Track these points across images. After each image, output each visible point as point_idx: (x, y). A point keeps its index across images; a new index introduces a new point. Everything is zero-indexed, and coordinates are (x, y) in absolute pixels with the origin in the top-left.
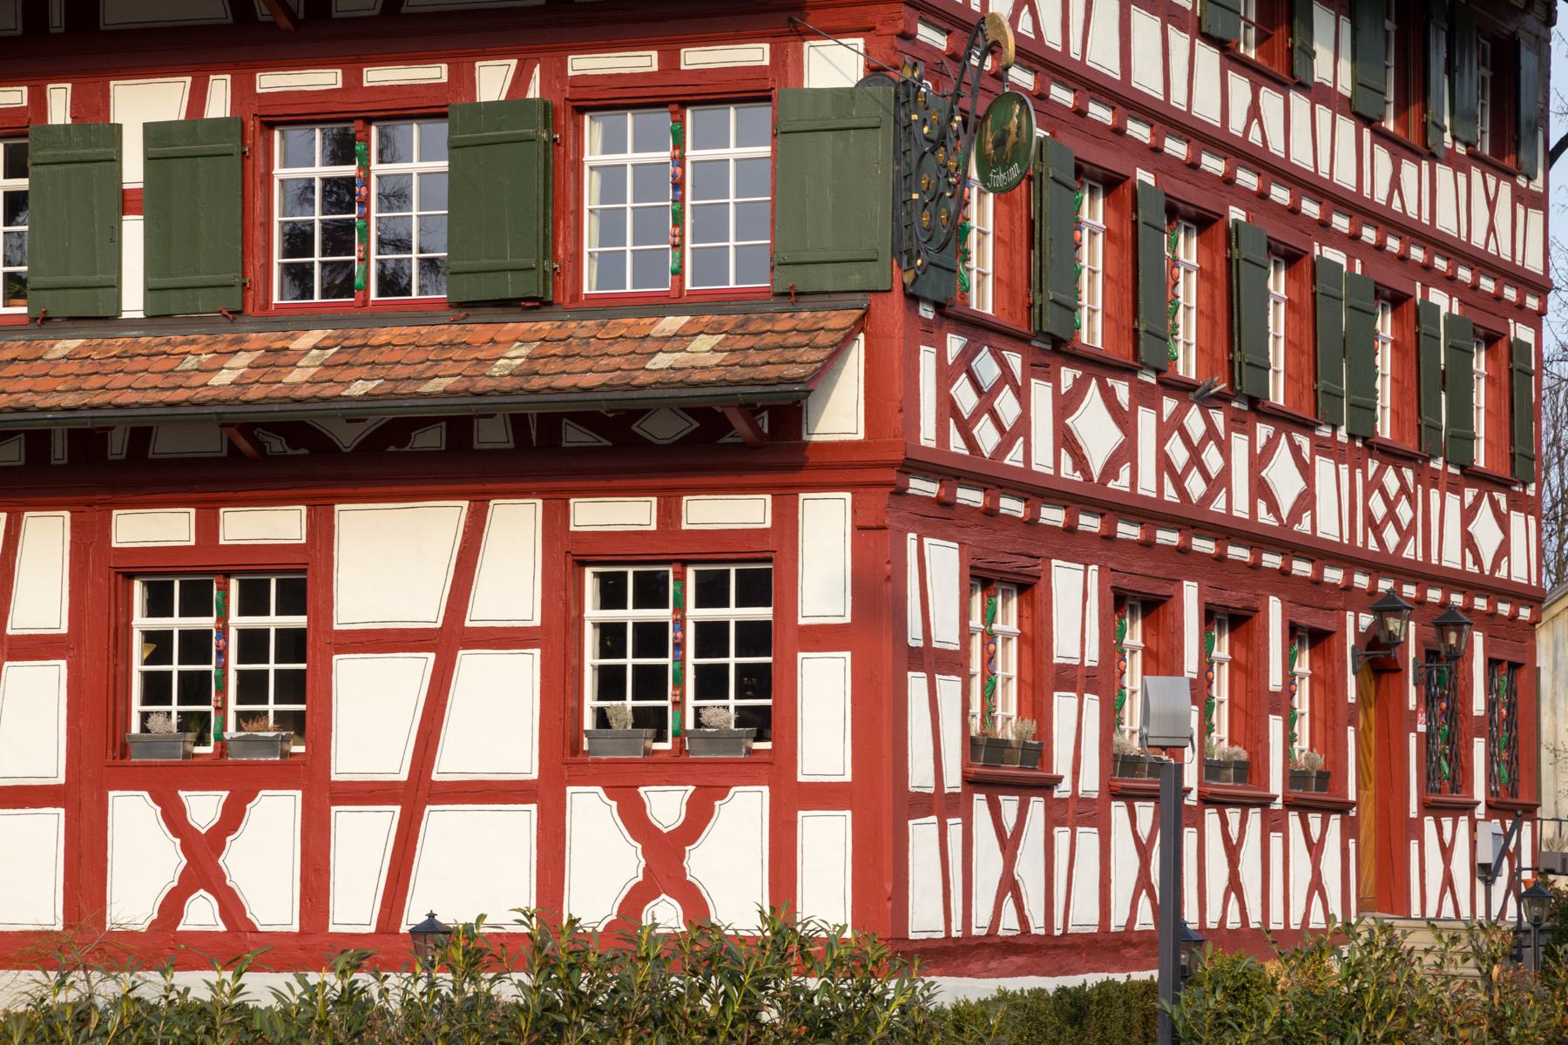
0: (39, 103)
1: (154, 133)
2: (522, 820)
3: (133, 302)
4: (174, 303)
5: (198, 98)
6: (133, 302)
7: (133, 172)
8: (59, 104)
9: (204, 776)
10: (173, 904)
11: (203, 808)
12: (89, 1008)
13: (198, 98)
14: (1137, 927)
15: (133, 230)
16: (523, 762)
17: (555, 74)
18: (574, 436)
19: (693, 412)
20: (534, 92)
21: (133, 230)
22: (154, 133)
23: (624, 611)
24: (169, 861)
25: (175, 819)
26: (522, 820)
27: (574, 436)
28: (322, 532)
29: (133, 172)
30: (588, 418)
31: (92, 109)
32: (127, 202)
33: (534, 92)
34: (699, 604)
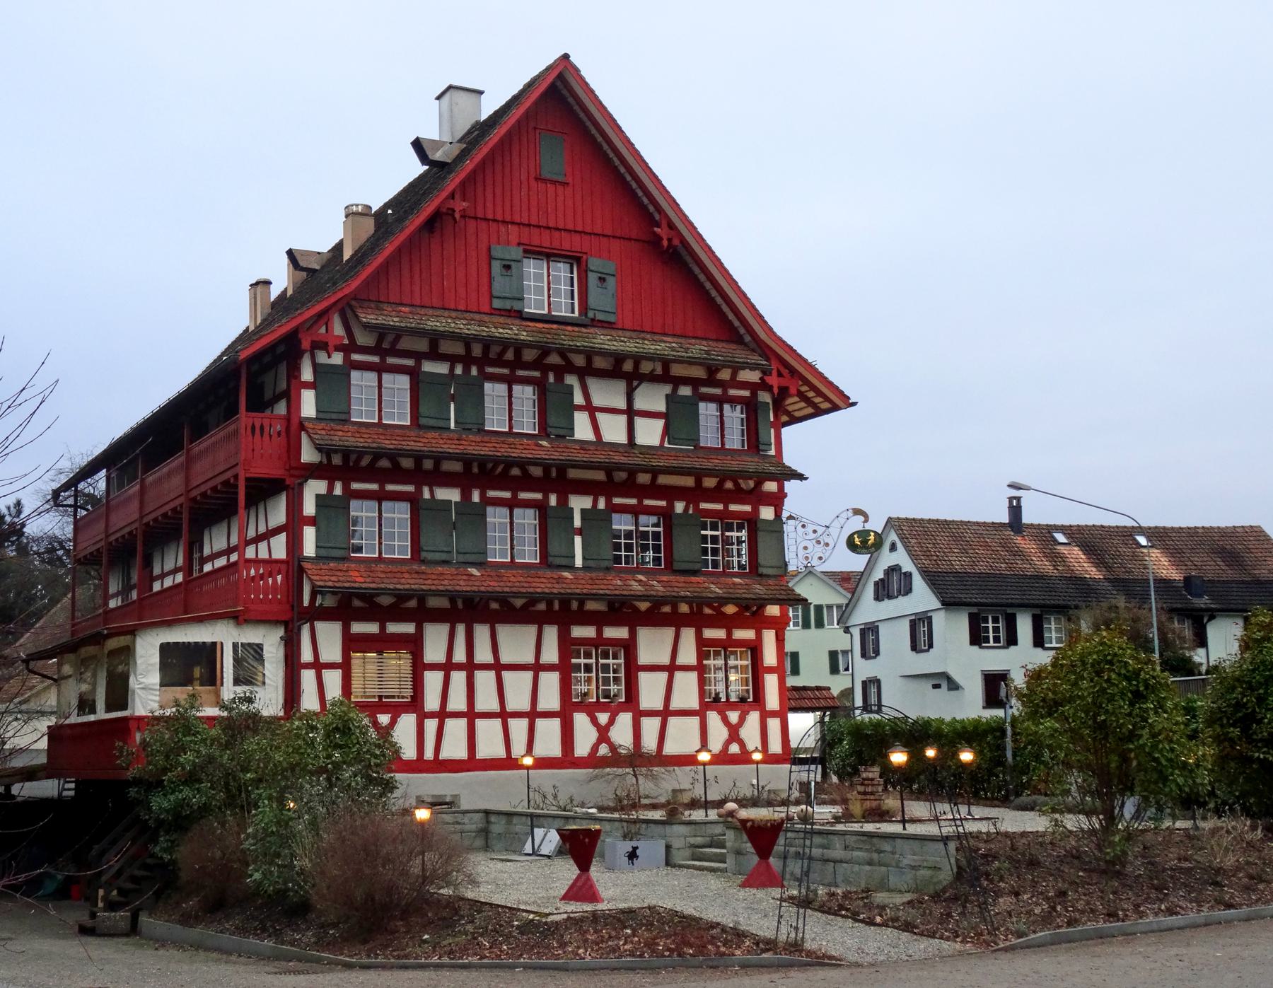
0: (546, 498)
1: (583, 511)
2: (695, 722)
3: (579, 562)
4: (591, 564)
5: (595, 503)
6: (579, 562)
7: (577, 522)
8: (553, 500)
9: (603, 708)
10: (595, 748)
11: (603, 718)
12: (1140, 671)
13: (595, 503)
14: (1211, 664)
15: (578, 541)
16: (694, 704)
17: (697, 508)
18: (357, 603)
19: (395, 595)
20: (691, 512)
21: (578, 541)
22: (583, 511)
23: (860, 654)
24: (593, 735)
25: (594, 721)
26: (695, 722)
27: (357, 603)
28: (633, 634)
29: (577, 522)
30: (361, 596)
31: (563, 502)
32: (580, 532)
33: (691, 512)
34: (989, 642)
